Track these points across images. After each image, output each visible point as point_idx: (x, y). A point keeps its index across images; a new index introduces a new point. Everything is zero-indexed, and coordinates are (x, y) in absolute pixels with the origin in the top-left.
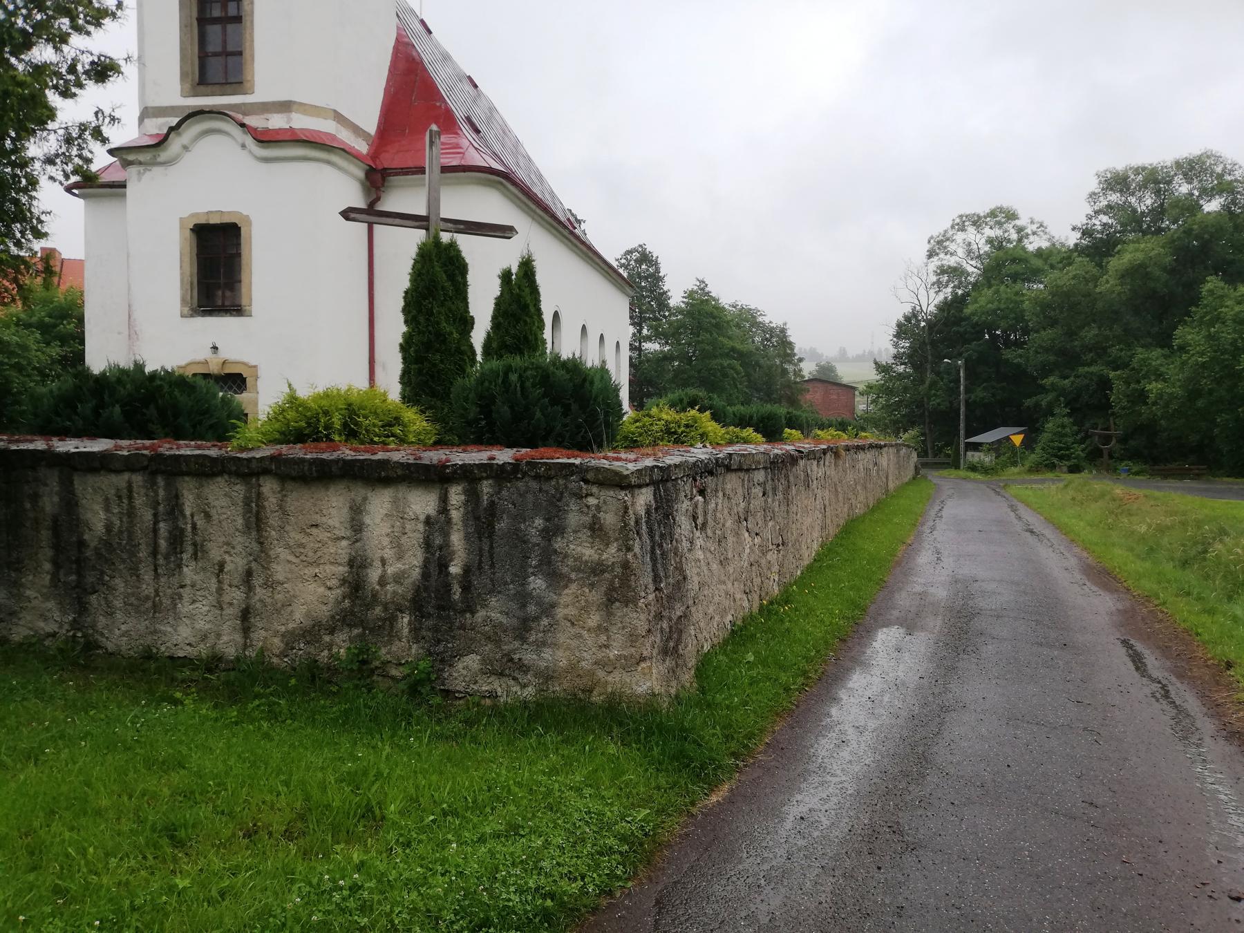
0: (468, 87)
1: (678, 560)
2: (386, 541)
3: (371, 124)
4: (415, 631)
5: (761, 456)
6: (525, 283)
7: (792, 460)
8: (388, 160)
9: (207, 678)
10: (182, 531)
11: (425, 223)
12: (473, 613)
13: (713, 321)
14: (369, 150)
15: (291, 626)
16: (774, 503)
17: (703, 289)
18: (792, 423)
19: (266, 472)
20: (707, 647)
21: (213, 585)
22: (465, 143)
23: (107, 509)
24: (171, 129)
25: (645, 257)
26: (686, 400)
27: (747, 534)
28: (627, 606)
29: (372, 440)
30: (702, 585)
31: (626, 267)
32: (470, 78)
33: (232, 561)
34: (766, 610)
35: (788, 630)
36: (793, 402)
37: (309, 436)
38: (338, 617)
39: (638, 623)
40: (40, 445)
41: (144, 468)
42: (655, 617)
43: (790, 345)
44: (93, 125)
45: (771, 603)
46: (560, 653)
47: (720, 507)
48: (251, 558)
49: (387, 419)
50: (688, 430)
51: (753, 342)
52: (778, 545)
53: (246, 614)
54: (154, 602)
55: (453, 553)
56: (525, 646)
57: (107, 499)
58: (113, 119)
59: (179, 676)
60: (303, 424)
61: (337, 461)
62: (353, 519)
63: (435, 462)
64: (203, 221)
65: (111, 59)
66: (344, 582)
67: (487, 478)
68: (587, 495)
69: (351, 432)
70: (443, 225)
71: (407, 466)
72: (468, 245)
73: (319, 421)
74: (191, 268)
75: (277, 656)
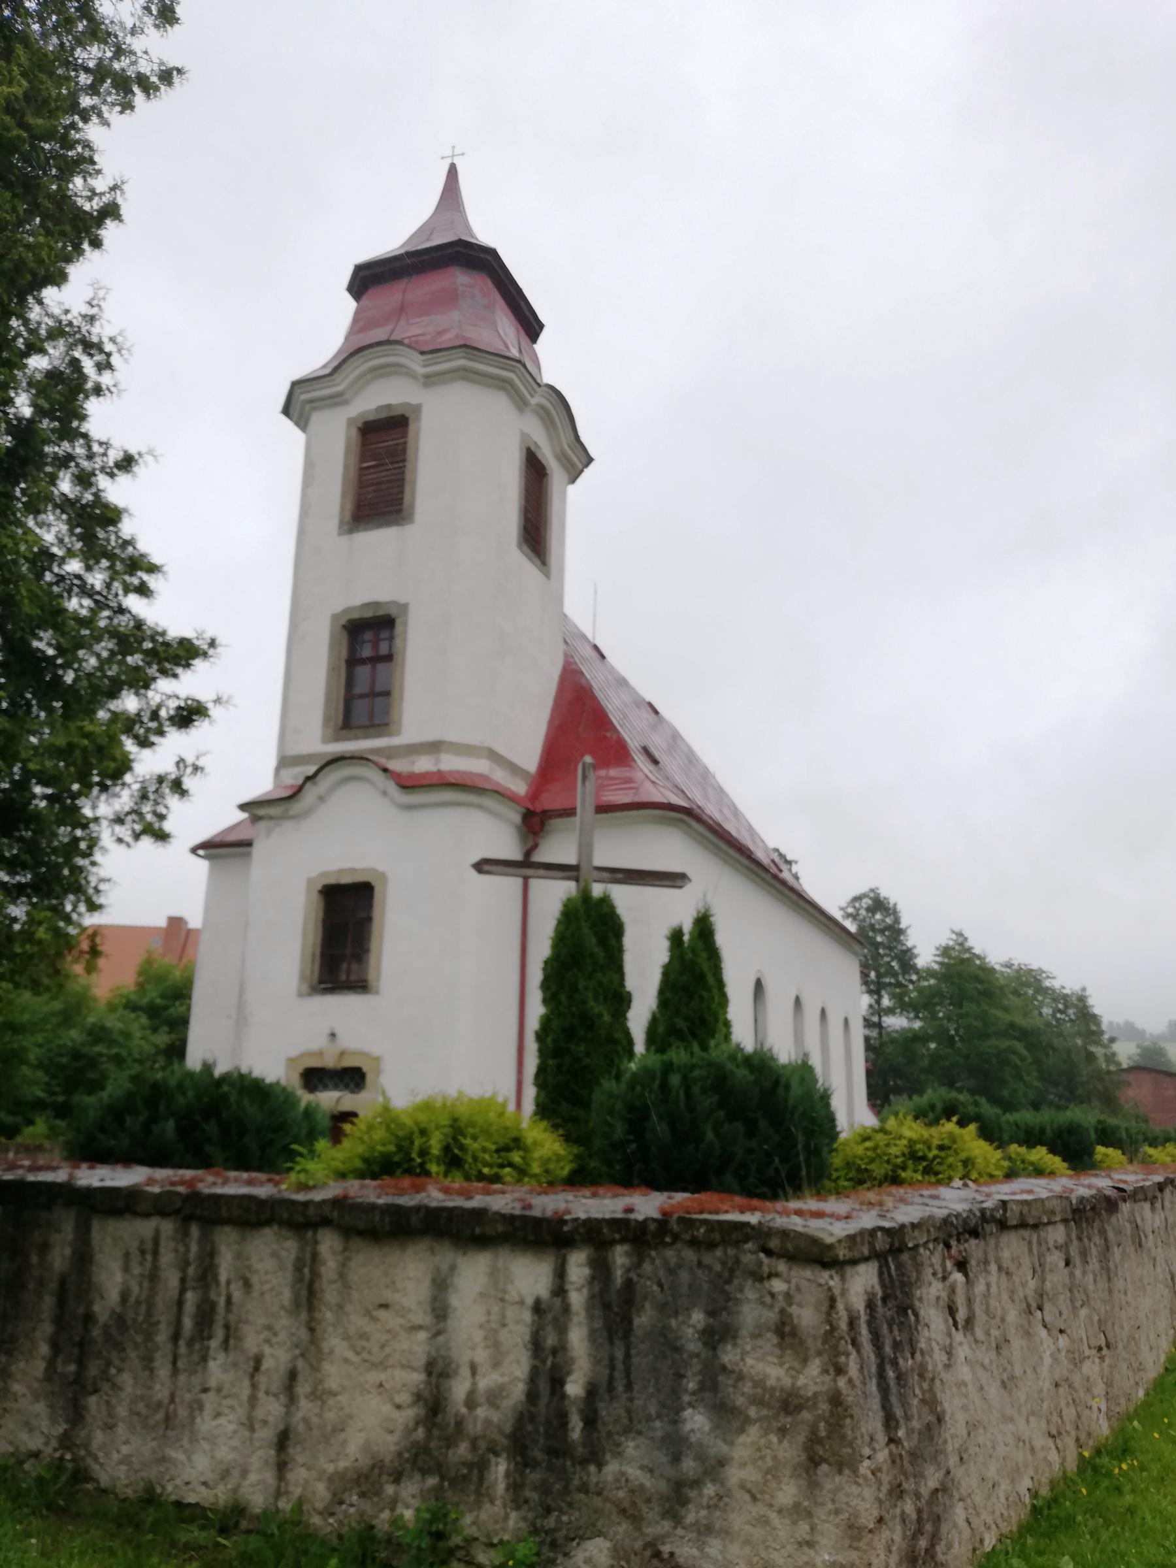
0: (647, 715)
1: (925, 1386)
2: (478, 1336)
3: (530, 760)
4: (515, 1487)
5: (1055, 1202)
6: (700, 944)
7: (1108, 1204)
8: (548, 801)
9: (218, 1544)
10: (213, 1306)
11: (574, 874)
12: (600, 1465)
13: (979, 986)
14: (527, 792)
15: (343, 1464)
16: (1088, 1276)
17: (961, 944)
18: (1107, 1137)
19: (325, 1222)
20: (990, 1542)
21: (245, 1392)
22: (639, 776)
23: (126, 1269)
24: (308, 779)
25: (879, 904)
26: (939, 1106)
27: (1043, 1333)
28: (840, 1472)
29: (480, 1172)
30: (972, 1427)
31: (854, 917)
32: (651, 705)
33: (272, 1356)
34: (1090, 1468)
35: (1131, 1510)
36: (1109, 1102)
37: (398, 1165)
38: (406, 1455)
39: (862, 1506)
40: (60, 1176)
41: (176, 1213)
42: (890, 1492)
43: (1095, 1019)
44: (173, 776)
45: (1098, 1452)
46: (735, 1549)
47: (994, 1289)
48: (297, 1352)
49: (502, 1141)
50: (943, 1154)
51: (1041, 1014)
52: (1100, 1349)
53: (283, 1440)
54: (167, 1412)
55: (572, 1361)
56: (680, 1531)
57: (127, 1255)
58: (196, 769)
59: (183, 1537)
60: (392, 1148)
61: (417, 1209)
62: (435, 1299)
63: (549, 1214)
64: (332, 881)
65: (198, 701)
66: (418, 1397)
67: (623, 1241)
68: (770, 1276)
69: (453, 1160)
70: (596, 874)
71: (510, 1219)
72: (624, 898)
73: (412, 1143)
74: (315, 937)
75: (321, 1513)
